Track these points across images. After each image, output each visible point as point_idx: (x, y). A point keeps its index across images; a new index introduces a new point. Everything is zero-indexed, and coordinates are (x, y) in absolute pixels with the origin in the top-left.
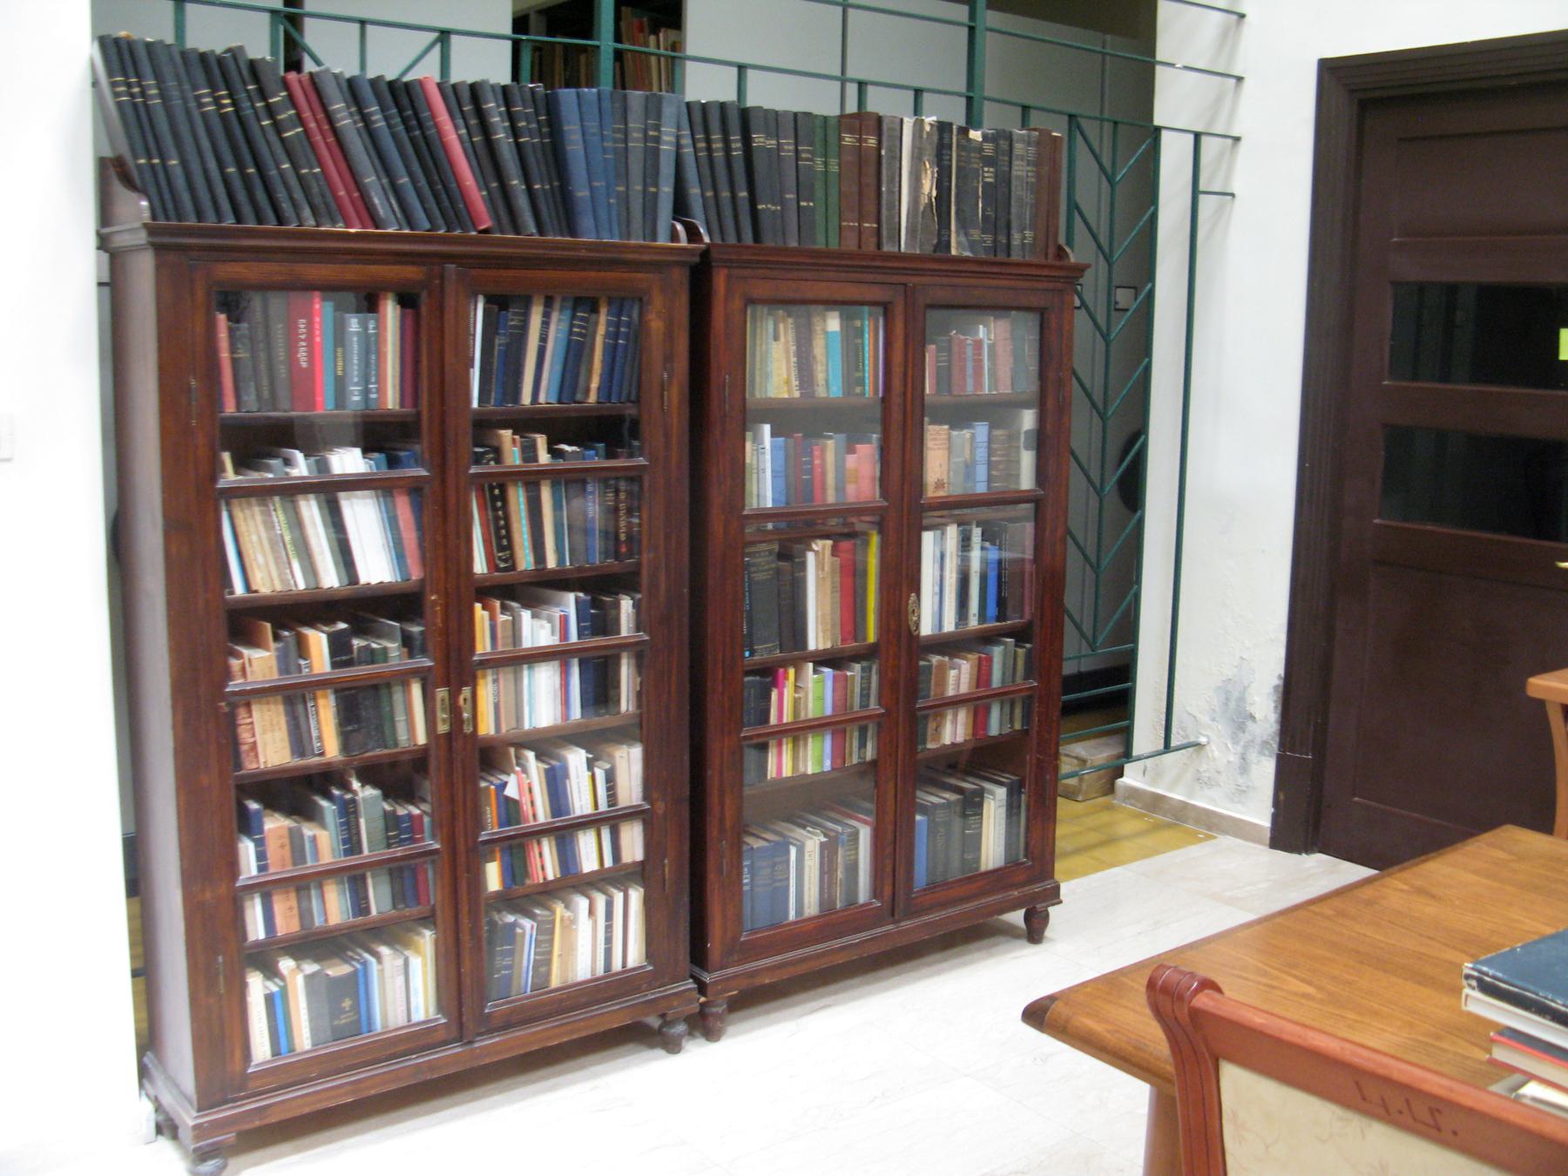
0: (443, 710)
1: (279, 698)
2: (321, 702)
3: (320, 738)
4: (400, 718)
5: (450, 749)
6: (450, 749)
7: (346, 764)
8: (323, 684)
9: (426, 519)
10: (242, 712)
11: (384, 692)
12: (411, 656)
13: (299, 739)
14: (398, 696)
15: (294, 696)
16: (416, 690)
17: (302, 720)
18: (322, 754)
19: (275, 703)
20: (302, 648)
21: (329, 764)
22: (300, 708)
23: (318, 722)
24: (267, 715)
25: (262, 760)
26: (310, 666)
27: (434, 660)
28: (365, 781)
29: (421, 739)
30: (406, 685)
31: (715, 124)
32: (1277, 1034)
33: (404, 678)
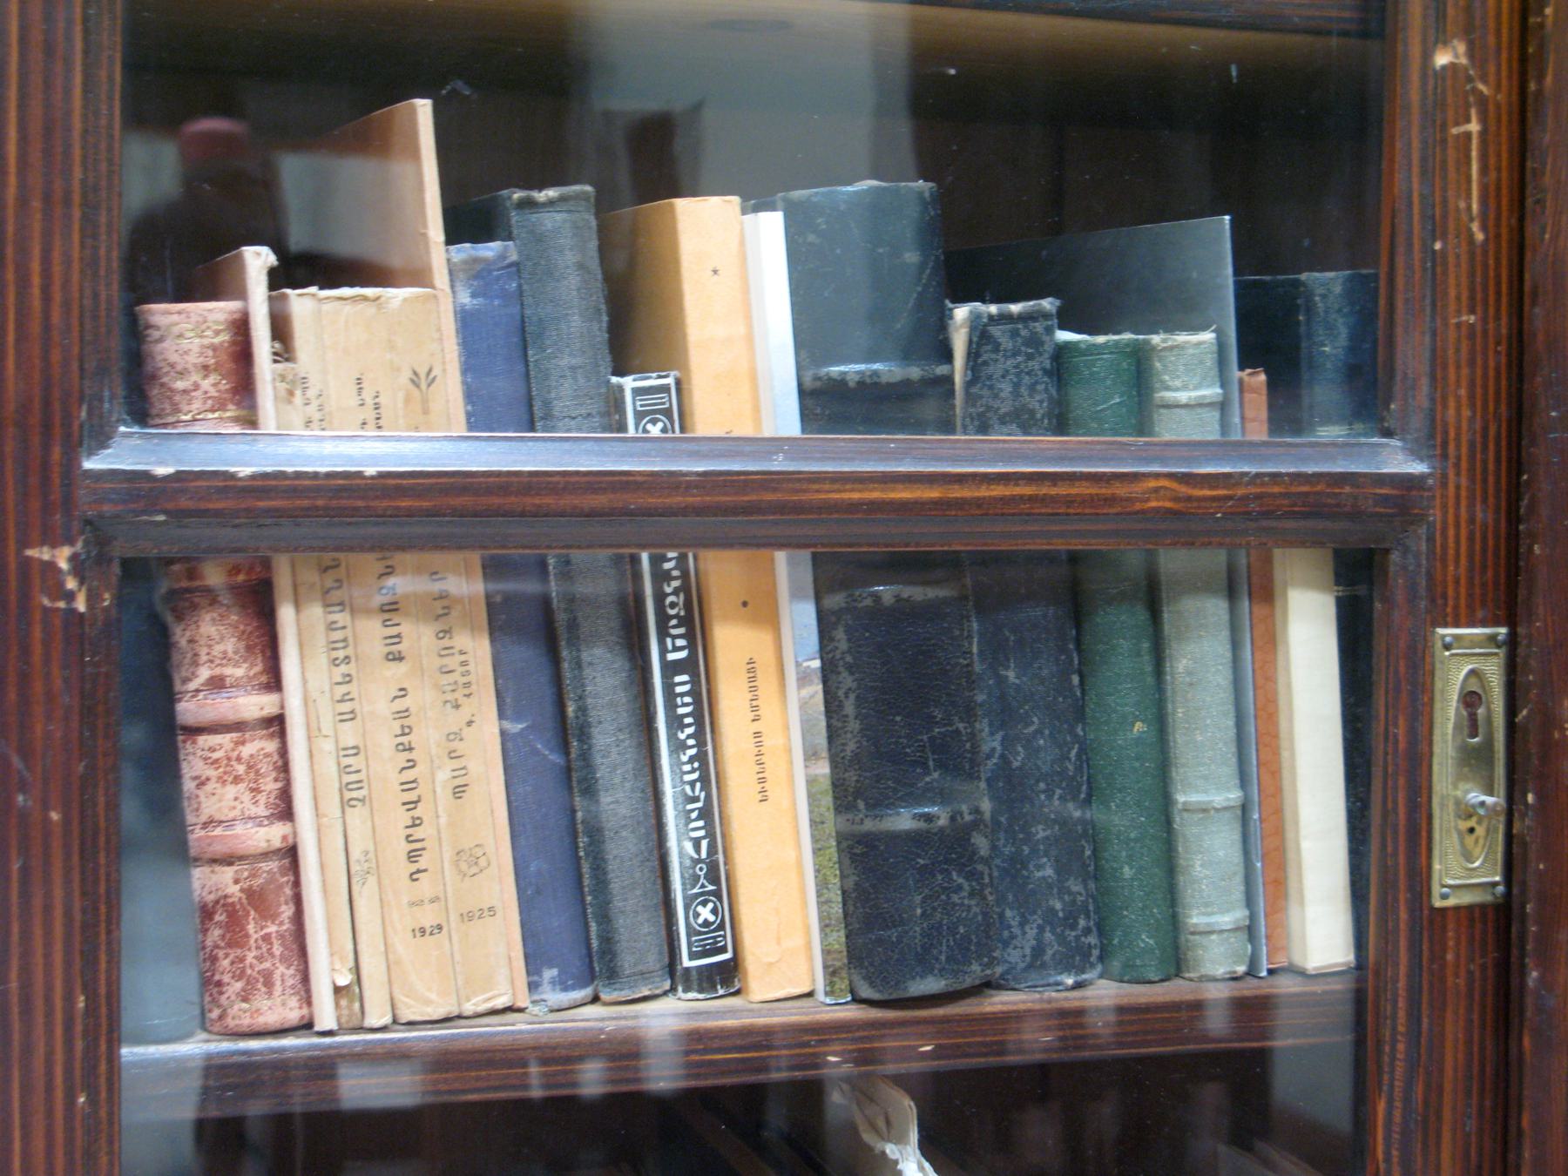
0: (1474, 760)
1: (466, 584)
2: (733, 643)
3: (716, 876)
4: (1205, 787)
5: (1504, 1006)
6: (1504, 1006)
7: (863, 1045)
8: (742, 508)
9: (1334, 42)
10: (213, 642)
11: (1119, 627)
12: (1287, 410)
13: (587, 882)
14: (1201, 654)
15: (570, 589)
16: (1309, 630)
17: (610, 743)
18: (725, 975)
19: (441, 610)
20: (636, 317)
21: (758, 1039)
22: (600, 677)
23: (708, 771)
24: (378, 691)
25: (327, 971)
26: (679, 414)
27: (1434, 441)
28: (86, 767)
29: (1322, 935)
30: (1251, 591)
31: (1463, 610)
32: (532, 1043)
33: (1242, 533)
